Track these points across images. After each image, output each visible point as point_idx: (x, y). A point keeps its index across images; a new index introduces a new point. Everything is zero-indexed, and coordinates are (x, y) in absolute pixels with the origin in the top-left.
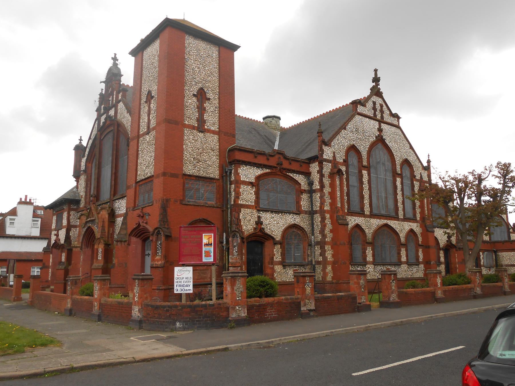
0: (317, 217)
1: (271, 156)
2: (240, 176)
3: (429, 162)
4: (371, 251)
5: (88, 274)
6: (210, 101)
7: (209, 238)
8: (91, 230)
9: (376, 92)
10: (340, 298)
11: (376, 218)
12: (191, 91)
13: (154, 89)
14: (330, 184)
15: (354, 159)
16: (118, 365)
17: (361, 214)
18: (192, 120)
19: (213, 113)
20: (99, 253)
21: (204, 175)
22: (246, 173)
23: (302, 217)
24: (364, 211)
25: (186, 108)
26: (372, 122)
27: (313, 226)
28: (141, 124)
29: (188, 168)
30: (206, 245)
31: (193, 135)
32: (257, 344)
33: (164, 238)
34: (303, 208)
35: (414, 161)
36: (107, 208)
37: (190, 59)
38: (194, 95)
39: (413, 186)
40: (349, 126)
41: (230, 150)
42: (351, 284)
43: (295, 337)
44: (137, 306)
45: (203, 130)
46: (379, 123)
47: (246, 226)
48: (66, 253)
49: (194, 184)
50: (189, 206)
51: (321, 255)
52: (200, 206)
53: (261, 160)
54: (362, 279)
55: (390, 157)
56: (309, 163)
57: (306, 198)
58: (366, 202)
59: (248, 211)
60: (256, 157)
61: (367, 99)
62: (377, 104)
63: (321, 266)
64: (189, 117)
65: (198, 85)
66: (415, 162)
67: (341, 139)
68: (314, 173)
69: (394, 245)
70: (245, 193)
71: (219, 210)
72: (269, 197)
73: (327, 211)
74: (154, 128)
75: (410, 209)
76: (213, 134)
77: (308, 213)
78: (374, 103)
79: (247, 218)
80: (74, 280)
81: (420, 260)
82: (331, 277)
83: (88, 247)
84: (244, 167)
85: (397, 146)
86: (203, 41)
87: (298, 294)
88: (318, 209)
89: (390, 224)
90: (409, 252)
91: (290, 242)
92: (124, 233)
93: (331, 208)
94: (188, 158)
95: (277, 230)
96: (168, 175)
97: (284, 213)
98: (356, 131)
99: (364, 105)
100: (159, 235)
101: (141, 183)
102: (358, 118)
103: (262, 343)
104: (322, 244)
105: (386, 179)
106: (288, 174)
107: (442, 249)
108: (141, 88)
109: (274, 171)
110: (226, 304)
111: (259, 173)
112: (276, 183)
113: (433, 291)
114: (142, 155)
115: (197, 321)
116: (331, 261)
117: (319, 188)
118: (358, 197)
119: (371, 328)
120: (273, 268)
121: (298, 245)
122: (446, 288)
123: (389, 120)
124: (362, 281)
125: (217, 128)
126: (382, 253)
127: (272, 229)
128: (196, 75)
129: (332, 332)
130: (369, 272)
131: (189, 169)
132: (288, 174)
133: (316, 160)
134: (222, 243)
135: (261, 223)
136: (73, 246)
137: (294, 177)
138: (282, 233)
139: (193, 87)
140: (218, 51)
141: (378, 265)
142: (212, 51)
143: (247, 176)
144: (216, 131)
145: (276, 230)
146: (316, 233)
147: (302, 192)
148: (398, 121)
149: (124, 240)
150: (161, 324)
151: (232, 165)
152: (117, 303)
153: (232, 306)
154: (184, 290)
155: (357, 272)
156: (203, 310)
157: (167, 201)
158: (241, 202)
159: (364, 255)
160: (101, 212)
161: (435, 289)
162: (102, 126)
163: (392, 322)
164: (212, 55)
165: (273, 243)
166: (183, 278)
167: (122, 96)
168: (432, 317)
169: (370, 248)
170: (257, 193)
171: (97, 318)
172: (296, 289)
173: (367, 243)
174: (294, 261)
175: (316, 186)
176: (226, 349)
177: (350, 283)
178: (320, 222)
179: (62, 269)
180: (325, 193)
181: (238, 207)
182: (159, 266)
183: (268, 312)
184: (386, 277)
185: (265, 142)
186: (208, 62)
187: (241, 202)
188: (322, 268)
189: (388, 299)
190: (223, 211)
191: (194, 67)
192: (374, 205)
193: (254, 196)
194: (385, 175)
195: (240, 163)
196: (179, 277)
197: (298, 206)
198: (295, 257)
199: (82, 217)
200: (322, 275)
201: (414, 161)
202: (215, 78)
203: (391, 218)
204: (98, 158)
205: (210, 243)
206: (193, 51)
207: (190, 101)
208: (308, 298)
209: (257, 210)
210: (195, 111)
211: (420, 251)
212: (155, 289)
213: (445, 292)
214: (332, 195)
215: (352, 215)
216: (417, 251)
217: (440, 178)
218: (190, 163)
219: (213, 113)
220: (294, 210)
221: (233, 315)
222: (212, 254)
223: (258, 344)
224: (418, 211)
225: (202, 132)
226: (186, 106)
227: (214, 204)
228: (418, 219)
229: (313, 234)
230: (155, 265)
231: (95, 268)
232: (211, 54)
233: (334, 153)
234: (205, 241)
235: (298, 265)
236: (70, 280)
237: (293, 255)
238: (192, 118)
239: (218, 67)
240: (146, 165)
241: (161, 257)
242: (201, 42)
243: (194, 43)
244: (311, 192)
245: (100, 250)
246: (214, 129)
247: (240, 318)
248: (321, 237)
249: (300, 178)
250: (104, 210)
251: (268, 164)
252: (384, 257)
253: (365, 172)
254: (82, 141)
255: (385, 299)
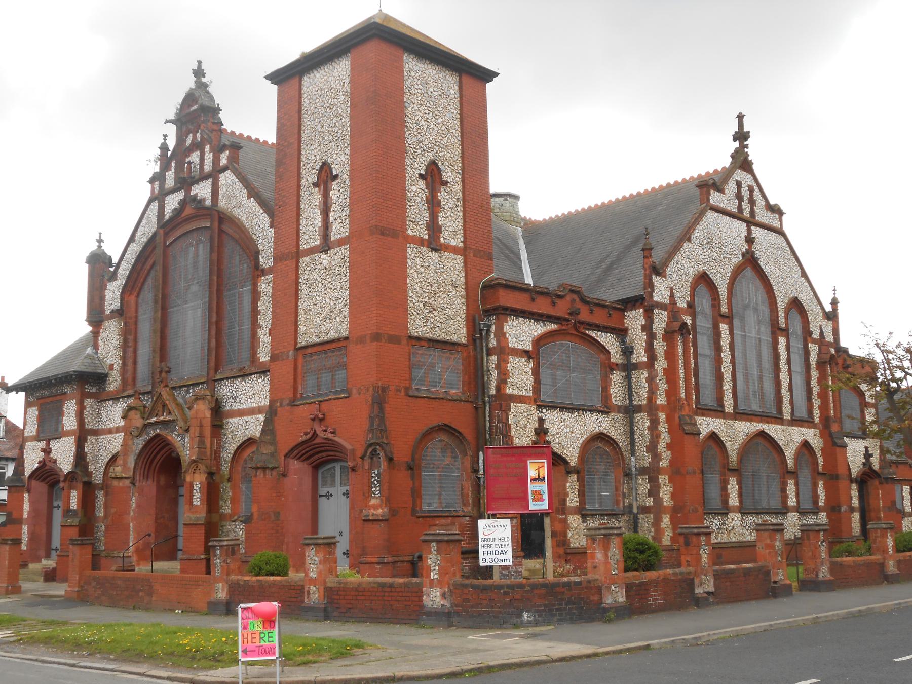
0: (642, 418)
1: (560, 297)
2: (508, 339)
3: (834, 302)
4: (737, 487)
5: (149, 535)
6: (447, 186)
7: (539, 468)
8: (160, 440)
9: (742, 161)
10: (747, 572)
11: (744, 420)
12: (415, 169)
13: (340, 163)
14: (666, 352)
15: (704, 301)
16: (535, 664)
17: (718, 411)
18: (418, 227)
19: (453, 211)
20: (195, 491)
21: (441, 337)
22: (517, 333)
23: (613, 419)
24: (723, 406)
25: (409, 204)
26: (736, 223)
27: (634, 437)
28: (302, 229)
29: (415, 323)
30: (534, 479)
31: (421, 256)
32: (682, 641)
33: (385, 464)
34: (613, 400)
35: (808, 302)
36: (208, 397)
37: (412, 102)
38: (421, 176)
39: (807, 353)
40: (697, 234)
41: (485, 287)
42: (759, 548)
43: (726, 632)
44: (436, 587)
45: (437, 246)
46: (747, 226)
47: (519, 439)
48: (81, 491)
49: (426, 354)
50: (419, 399)
51: (650, 494)
52: (439, 399)
53: (542, 306)
54: (778, 540)
55: (767, 294)
56: (624, 310)
57: (619, 381)
58: (727, 387)
59: (523, 407)
60: (533, 300)
61: (727, 174)
62: (743, 186)
63: (652, 516)
64: (414, 220)
65: (426, 155)
66: (811, 304)
67: (683, 262)
68: (634, 331)
69: (776, 473)
70: (517, 373)
71: (469, 407)
72: (555, 379)
73: (662, 408)
74: (341, 242)
75: (802, 399)
76: (455, 254)
77: (623, 411)
78: (739, 185)
79: (521, 422)
80: (230, 545)
81: (820, 504)
82: (669, 538)
83: (147, 478)
84: (513, 320)
85: (778, 271)
86: (432, 64)
87: (689, 566)
88: (644, 402)
89: (768, 432)
90: (800, 488)
91: (592, 470)
92: (270, 452)
93: (668, 401)
94: (414, 304)
95: (571, 445)
96: (384, 338)
97: (583, 410)
98: (708, 243)
99: (721, 191)
100: (375, 458)
101: (309, 351)
102: (711, 216)
103: (688, 639)
104: (652, 473)
105: (760, 340)
106: (587, 332)
107: (855, 481)
108: (299, 154)
109: (564, 328)
110: (598, 582)
111: (539, 332)
112: (567, 352)
113: (881, 561)
114: (310, 294)
115: (557, 610)
116: (669, 507)
117: (646, 360)
118: (712, 378)
119: (820, 620)
120: (565, 521)
121: (606, 475)
122: (901, 556)
123: (764, 218)
124: (778, 543)
125: (461, 242)
126: (754, 490)
127: (563, 444)
128: (422, 134)
129: (771, 625)
130: (733, 527)
131: (418, 327)
132: (587, 332)
133: (638, 304)
134: (476, 471)
135: (545, 431)
136: (113, 475)
137: (598, 339)
138: (580, 450)
139: (418, 160)
140: (458, 83)
141: (749, 513)
142: (447, 85)
143: (520, 339)
144: (459, 248)
145: (569, 446)
146: (640, 450)
147: (612, 367)
148: (780, 220)
149: (270, 466)
150: (495, 617)
151: (490, 315)
152: (376, 585)
153: (606, 585)
154: (496, 560)
155: (771, 528)
156: (566, 592)
157: (384, 389)
158: (509, 391)
159: (723, 493)
160: (195, 406)
161: (884, 559)
162: (171, 219)
163: (846, 610)
164: (448, 93)
165: (564, 472)
166: (494, 539)
167: (229, 159)
168: (900, 604)
169: (735, 479)
170: (536, 373)
171: (322, 614)
172: (683, 557)
173: (728, 470)
174: (599, 506)
175: (640, 357)
176: (648, 647)
177: (756, 546)
178: (649, 428)
179: (74, 526)
180: (657, 370)
181: (504, 401)
182: (381, 518)
183: (652, 596)
184: (812, 535)
185: (502, 253)
186: (443, 106)
187: (511, 390)
188: (652, 521)
189: (814, 576)
190: (476, 408)
191: (419, 119)
192: (740, 395)
193: (532, 378)
194: (759, 332)
195: (508, 313)
196: (487, 537)
197: (606, 396)
198: (601, 499)
199: (132, 414)
200: (652, 534)
201: (808, 302)
202: (454, 140)
203: (769, 419)
204: (160, 287)
205: (541, 476)
206: (416, 86)
207: (414, 188)
208: (705, 572)
209: (537, 405)
210: (423, 209)
211: (821, 484)
212: (375, 563)
213: (899, 563)
214: (670, 374)
215: (703, 415)
216: (815, 486)
217: (877, 345)
218: (418, 314)
219: (453, 211)
220: (598, 403)
221: (608, 600)
222: (546, 497)
223: (684, 641)
224: (816, 403)
225: (435, 250)
226: (409, 199)
227: (460, 394)
228: (817, 420)
229: (633, 453)
230: (373, 515)
231: (191, 522)
232: (446, 91)
233: (671, 289)
234: (532, 472)
235: (607, 515)
236: (221, 546)
237: (597, 494)
238: (420, 223)
239: (459, 116)
240: (323, 315)
241: (382, 500)
242: (430, 66)
243: (418, 68)
244: (628, 368)
245: (197, 486)
246: (455, 244)
247: (618, 605)
248: (650, 459)
249: (608, 340)
250: (200, 402)
251: (554, 314)
252: (757, 498)
253: (724, 327)
254: (102, 243)
255: (809, 576)
